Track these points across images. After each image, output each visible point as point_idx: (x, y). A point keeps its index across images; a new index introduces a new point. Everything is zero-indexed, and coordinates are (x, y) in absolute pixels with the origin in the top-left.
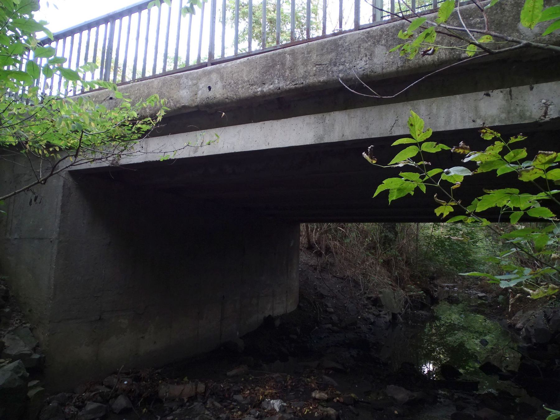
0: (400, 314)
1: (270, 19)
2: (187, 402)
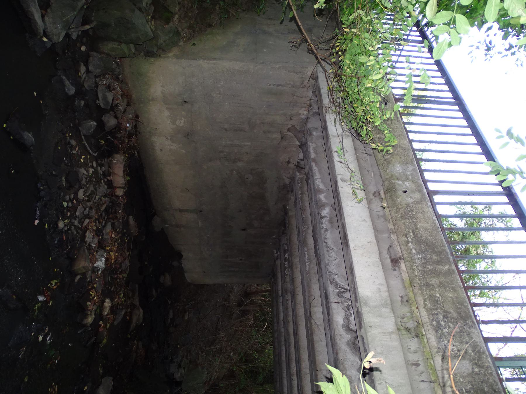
0: (181, 389)
1: (469, 249)
2: (108, 180)
